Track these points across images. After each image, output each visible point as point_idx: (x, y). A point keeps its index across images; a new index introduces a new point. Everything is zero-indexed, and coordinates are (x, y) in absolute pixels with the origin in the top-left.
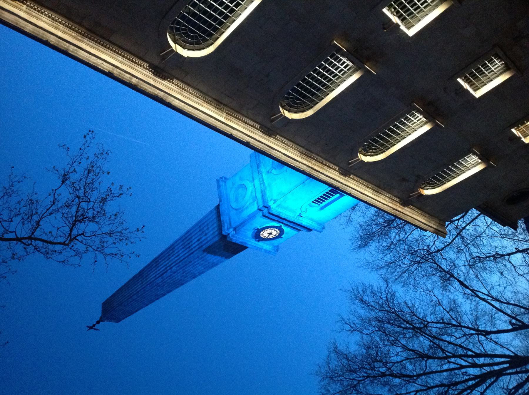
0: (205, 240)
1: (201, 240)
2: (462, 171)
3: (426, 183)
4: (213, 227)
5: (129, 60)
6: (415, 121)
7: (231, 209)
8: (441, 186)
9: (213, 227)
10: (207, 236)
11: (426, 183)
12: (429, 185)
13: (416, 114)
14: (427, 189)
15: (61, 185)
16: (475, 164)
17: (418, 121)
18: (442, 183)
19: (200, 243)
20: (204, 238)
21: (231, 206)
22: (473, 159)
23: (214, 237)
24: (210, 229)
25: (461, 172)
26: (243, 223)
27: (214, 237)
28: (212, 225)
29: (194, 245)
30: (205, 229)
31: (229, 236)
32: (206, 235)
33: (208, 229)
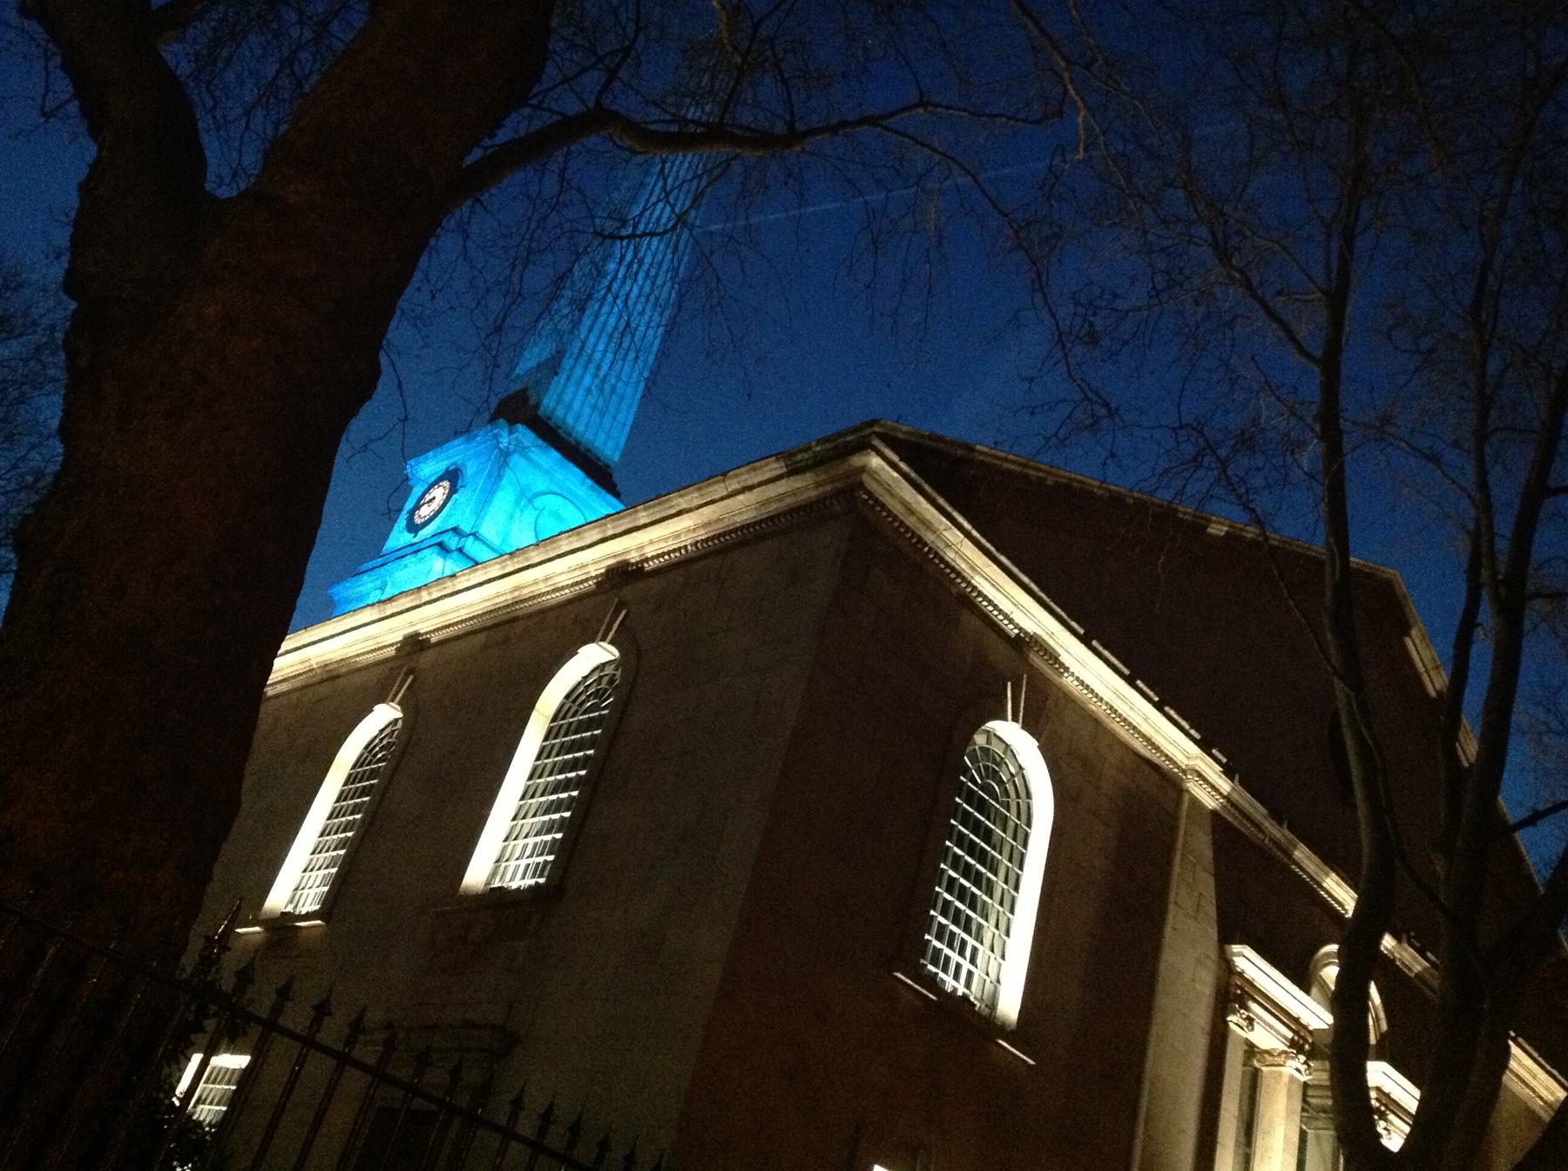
0: (582, 378)
1: (592, 369)
2: (329, 848)
3: (606, 690)
4: (584, 420)
5: (996, 607)
6: (523, 863)
7: (555, 489)
8: (554, 720)
9: (584, 420)
10: (581, 392)
11: (606, 690)
12: (385, 742)
13: (532, 882)
14: (382, 731)
15: (484, 542)
16: (503, 865)
17: (517, 867)
18: (555, 731)
19: (590, 361)
20: (587, 381)
21: (559, 495)
22: (518, 878)
23: (559, 401)
24: (588, 410)
25: (526, 807)
26: (496, 479)
27: (559, 401)
28: (589, 421)
29: (601, 347)
30: (601, 402)
31: (506, 430)
32: (589, 391)
33: (594, 407)
